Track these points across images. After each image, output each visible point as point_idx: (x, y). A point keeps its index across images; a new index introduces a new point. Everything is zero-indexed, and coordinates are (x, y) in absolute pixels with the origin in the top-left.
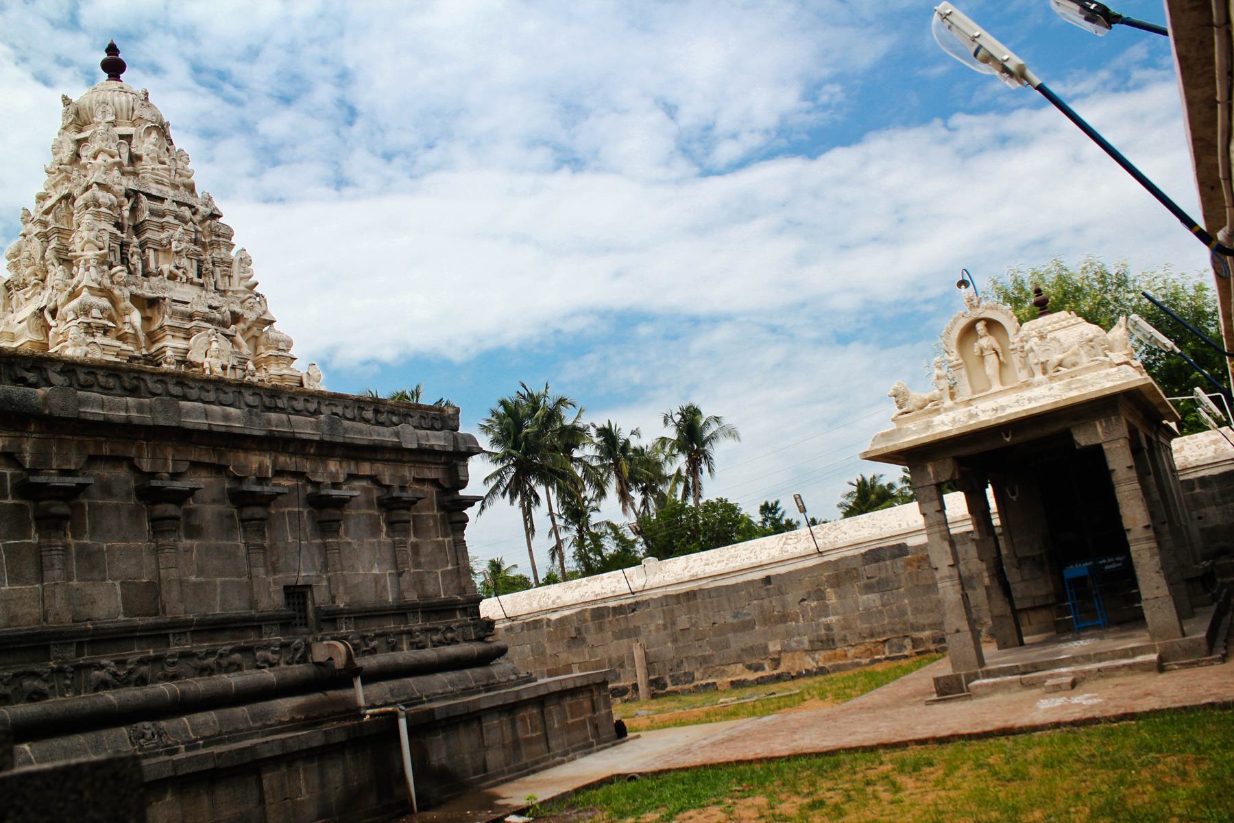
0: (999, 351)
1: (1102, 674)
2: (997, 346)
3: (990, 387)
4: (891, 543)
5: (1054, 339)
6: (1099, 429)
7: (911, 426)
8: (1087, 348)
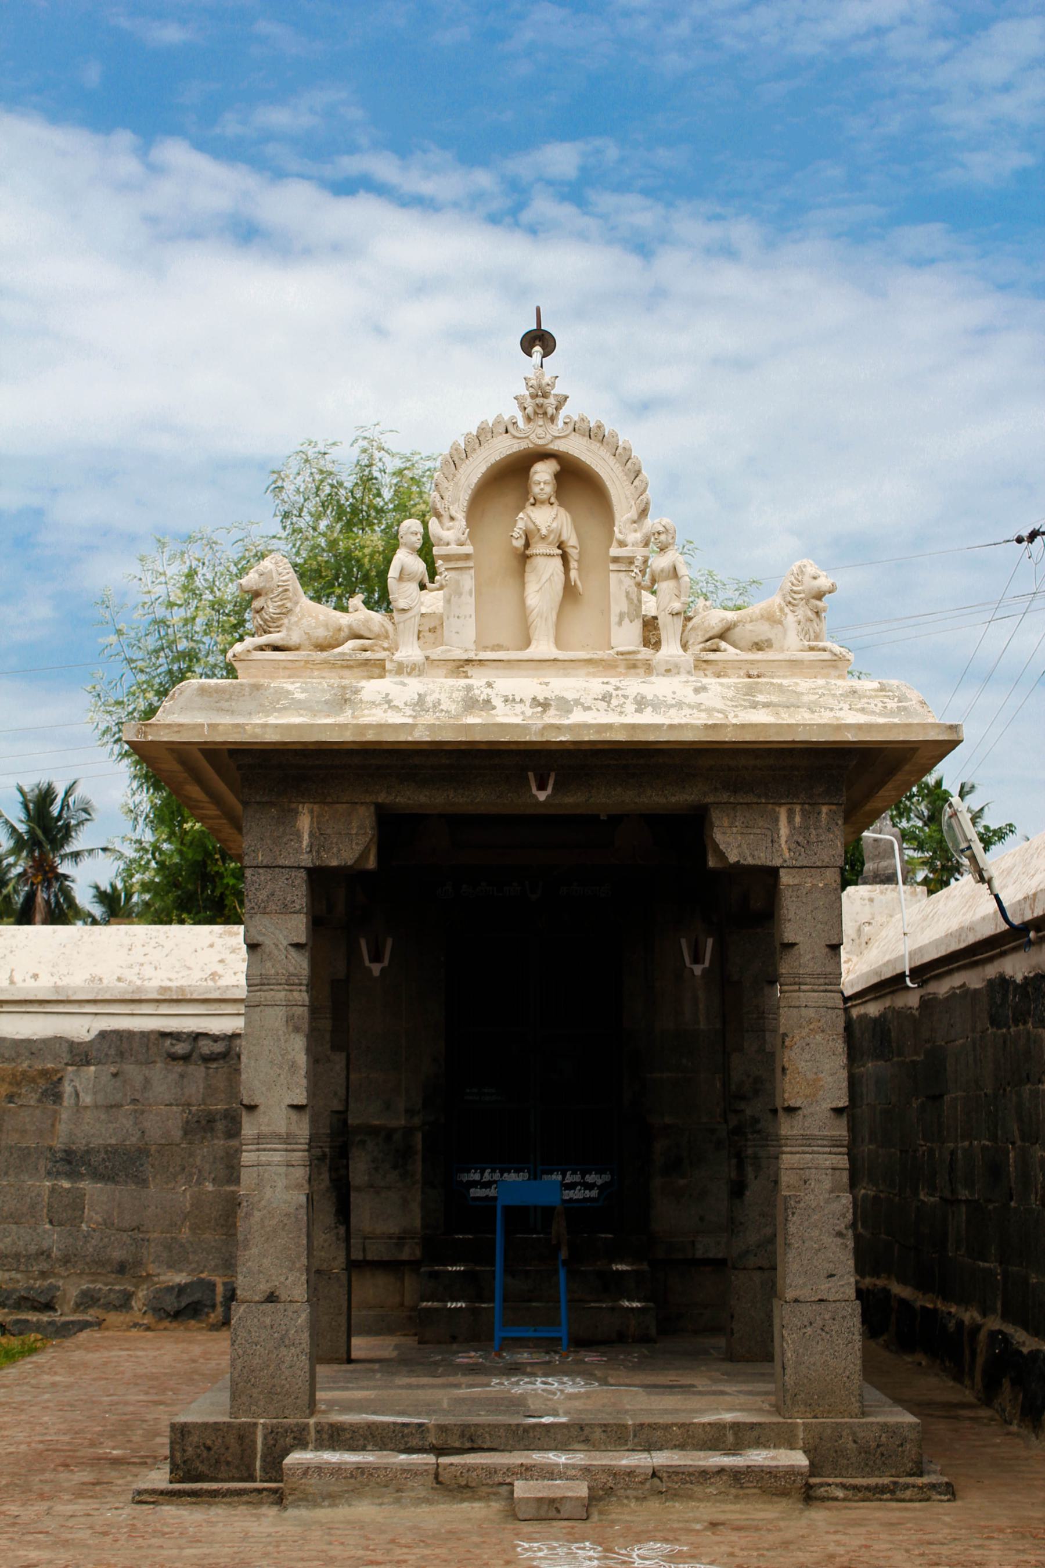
0: (574, 553)
1: (664, 1484)
2: (571, 540)
3: (527, 643)
6: (784, 831)
7: (294, 687)
8: (803, 611)
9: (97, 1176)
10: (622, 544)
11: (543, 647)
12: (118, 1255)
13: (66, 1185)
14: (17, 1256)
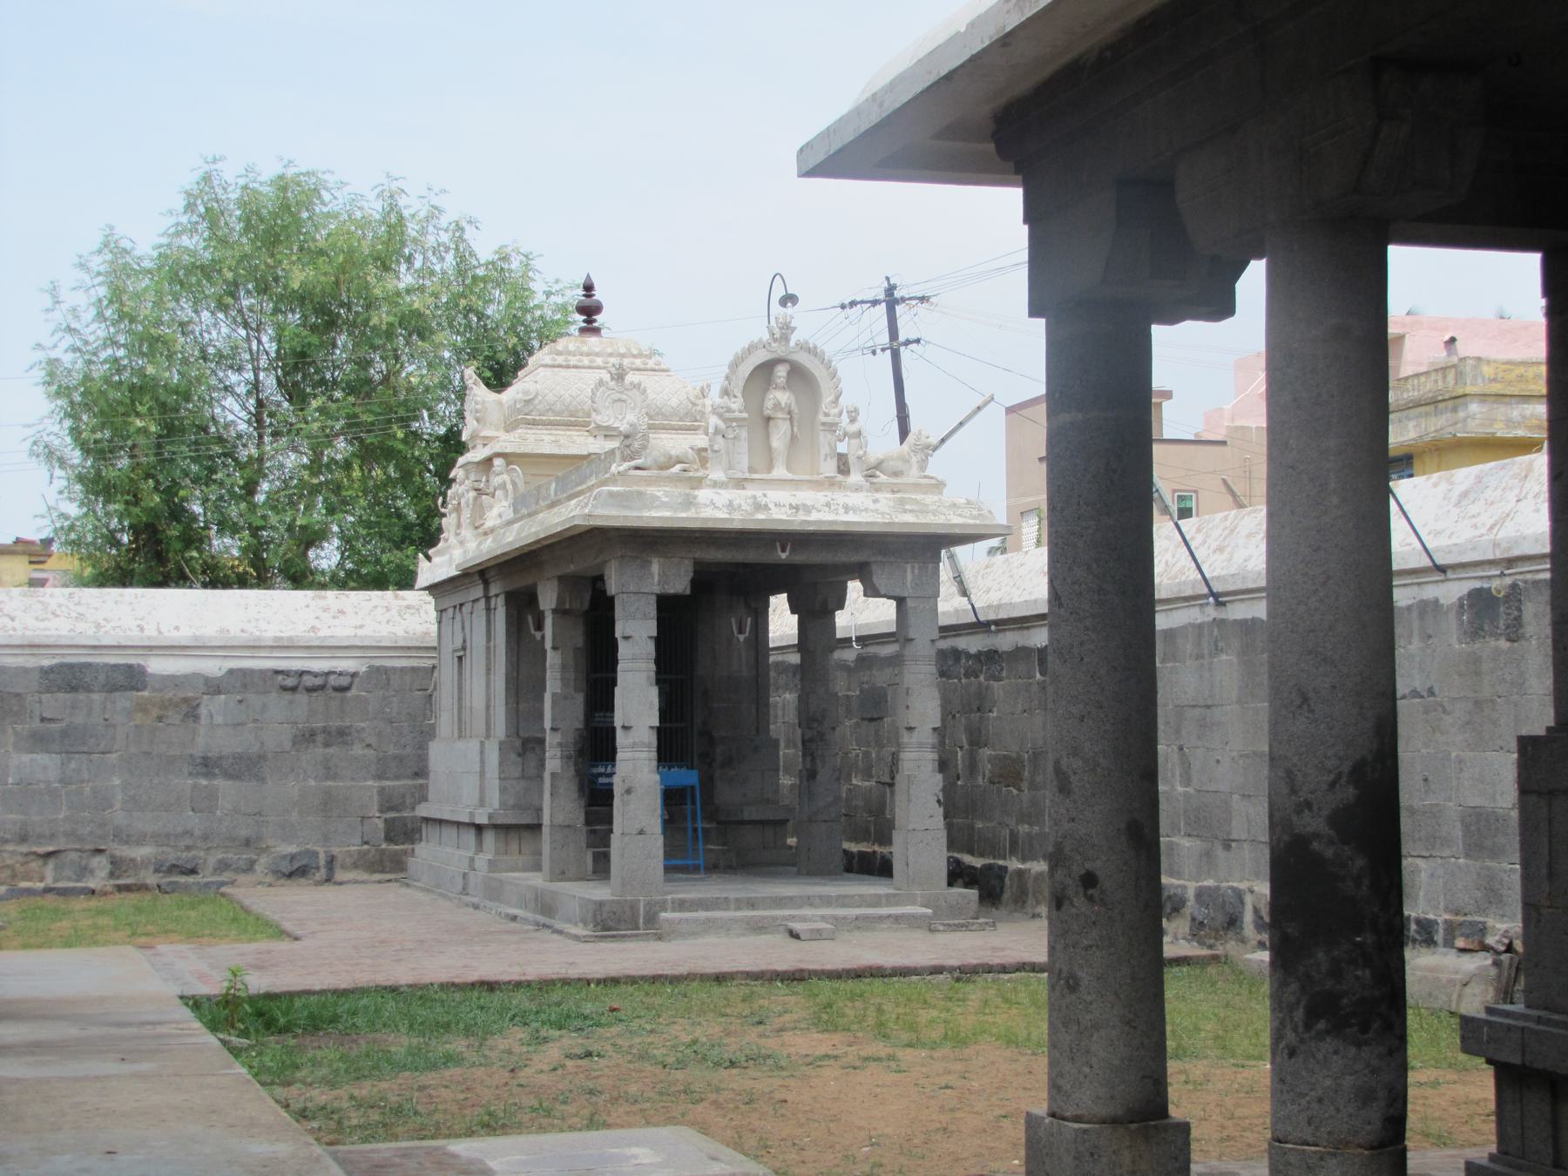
3: (770, 468)
4: (113, 660)
5: (637, 386)
6: (909, 577)
7: (659, 492)
9: (228, 775)
10: (827, 415)
11: (780, 472)
12: (244, 833)
13: (204, 782)
14: (168, 836)
